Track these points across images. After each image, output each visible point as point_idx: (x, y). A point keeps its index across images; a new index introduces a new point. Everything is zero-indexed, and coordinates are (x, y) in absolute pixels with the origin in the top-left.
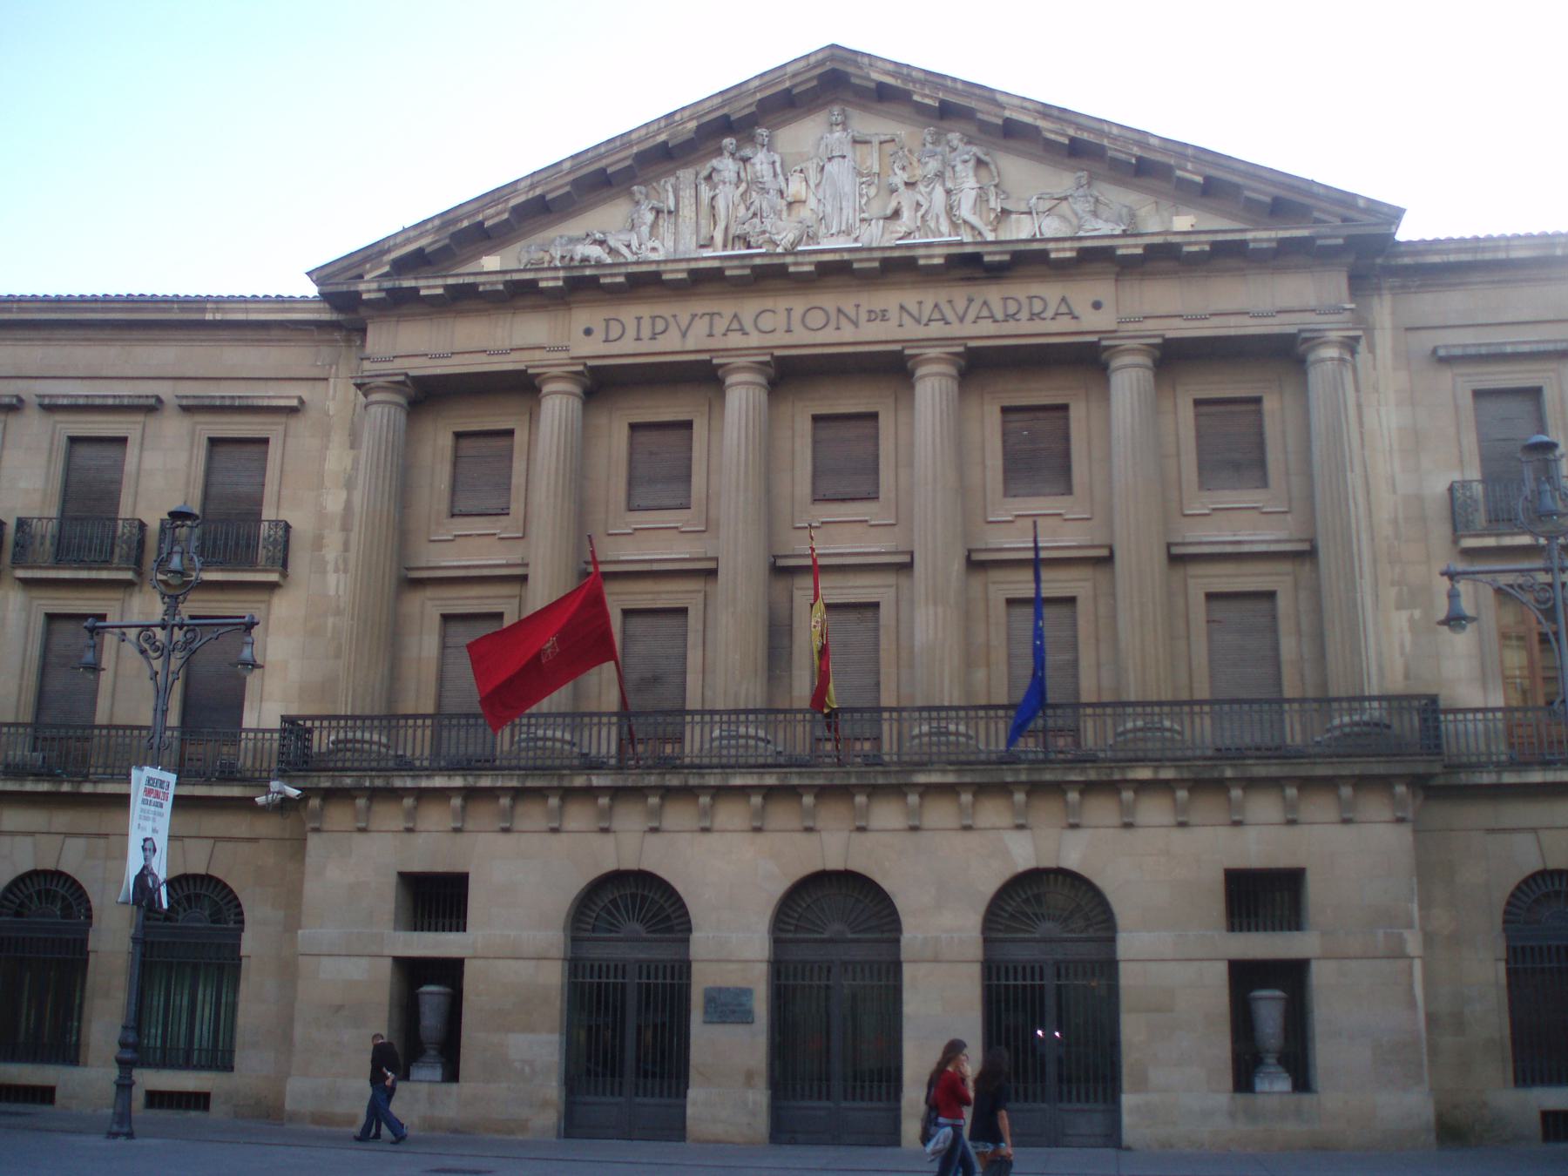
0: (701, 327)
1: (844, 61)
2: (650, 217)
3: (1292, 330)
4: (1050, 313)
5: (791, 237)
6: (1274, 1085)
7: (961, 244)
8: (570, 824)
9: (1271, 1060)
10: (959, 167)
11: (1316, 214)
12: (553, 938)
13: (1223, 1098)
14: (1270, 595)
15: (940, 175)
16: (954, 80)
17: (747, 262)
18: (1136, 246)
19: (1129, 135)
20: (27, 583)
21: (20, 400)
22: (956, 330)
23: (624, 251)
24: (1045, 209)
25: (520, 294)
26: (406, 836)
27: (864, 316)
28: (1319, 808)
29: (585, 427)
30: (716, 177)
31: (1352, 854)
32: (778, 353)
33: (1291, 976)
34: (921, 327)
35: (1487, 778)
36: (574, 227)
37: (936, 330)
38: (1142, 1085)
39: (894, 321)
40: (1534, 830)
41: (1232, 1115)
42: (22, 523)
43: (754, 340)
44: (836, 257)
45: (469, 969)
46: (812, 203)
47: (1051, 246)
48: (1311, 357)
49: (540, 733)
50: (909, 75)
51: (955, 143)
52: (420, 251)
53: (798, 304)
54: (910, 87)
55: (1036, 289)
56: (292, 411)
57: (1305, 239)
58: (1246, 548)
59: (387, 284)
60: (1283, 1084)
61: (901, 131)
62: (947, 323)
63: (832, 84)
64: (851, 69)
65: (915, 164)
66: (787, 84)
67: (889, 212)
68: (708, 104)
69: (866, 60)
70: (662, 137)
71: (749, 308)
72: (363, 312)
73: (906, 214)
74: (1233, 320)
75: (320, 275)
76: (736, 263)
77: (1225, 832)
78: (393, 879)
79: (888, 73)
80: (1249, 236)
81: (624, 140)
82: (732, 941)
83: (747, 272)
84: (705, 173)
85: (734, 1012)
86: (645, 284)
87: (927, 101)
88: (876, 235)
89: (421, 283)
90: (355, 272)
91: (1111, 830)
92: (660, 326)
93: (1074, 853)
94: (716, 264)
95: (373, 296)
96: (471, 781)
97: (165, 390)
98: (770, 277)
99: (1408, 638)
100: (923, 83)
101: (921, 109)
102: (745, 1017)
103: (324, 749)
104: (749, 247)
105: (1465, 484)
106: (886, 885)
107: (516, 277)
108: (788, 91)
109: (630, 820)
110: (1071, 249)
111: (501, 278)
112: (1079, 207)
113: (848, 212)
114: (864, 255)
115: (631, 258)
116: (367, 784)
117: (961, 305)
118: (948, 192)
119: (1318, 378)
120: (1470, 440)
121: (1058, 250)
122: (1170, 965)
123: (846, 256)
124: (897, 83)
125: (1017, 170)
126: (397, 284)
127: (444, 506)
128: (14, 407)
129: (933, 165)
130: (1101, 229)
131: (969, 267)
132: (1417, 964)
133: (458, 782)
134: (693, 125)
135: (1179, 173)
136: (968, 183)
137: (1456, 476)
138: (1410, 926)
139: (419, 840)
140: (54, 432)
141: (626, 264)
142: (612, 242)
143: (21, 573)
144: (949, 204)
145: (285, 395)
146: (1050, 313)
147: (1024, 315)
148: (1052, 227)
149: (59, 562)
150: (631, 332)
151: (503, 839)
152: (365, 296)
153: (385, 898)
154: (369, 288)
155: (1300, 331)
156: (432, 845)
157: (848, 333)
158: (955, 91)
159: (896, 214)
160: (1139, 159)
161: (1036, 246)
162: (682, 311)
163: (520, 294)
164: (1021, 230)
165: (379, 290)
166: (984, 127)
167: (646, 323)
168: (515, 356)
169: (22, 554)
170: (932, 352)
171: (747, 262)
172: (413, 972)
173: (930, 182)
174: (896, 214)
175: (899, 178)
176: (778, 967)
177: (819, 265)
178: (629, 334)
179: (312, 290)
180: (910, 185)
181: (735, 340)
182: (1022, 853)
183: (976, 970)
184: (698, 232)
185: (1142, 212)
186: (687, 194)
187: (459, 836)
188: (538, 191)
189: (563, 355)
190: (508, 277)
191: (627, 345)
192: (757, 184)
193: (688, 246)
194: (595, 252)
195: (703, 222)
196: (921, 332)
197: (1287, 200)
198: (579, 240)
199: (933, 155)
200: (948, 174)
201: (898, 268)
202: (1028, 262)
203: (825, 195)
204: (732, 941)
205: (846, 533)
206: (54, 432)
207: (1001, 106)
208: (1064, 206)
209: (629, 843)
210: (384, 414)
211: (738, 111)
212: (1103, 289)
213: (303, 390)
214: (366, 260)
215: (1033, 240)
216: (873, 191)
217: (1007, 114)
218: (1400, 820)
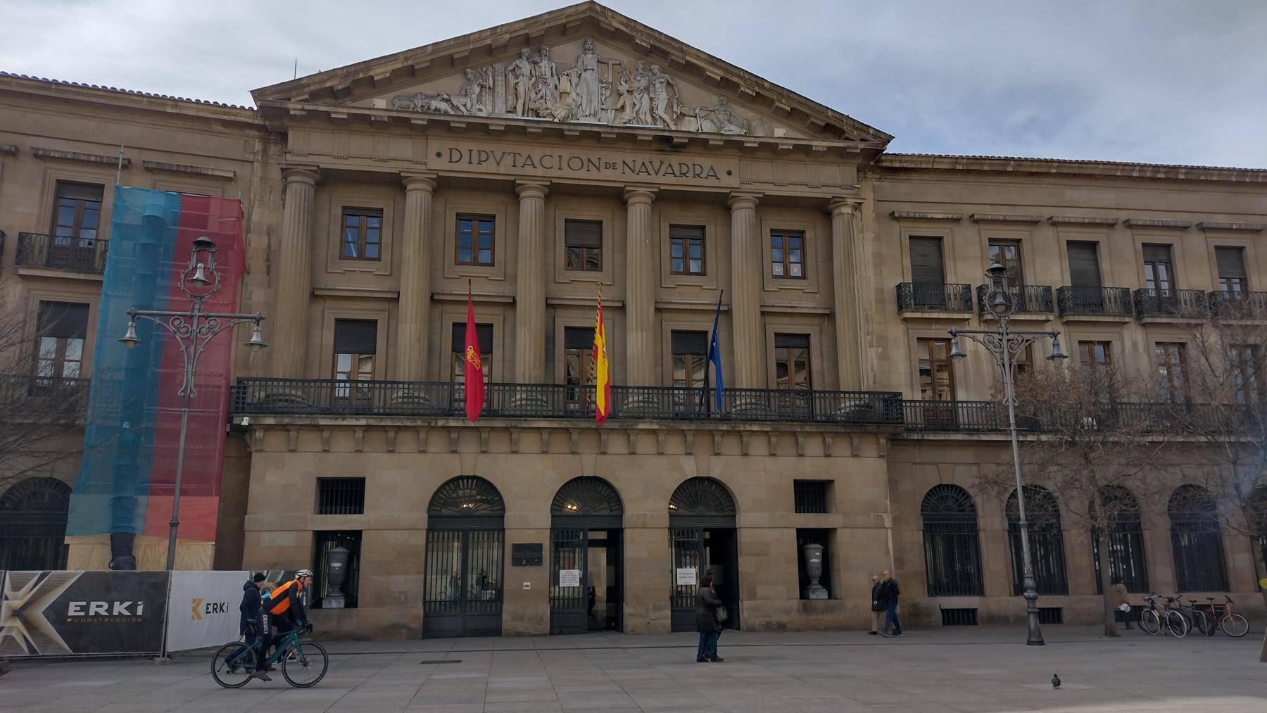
0: (508, 160)
2: (477, 90)
3: (829, 196)
4: (704, 175)
5: (563, 114)
6: (819, 594)
7: (657, 129)
8: (432, 449)
9: (815, 582)
10: (658, 85)
14: (807, 336)
15: (647, 89)
16: (661, 33)
20: (25, 278)
21: (17, 149)
22: (653, 178)
23: (462, 108)
24: (703, 117)
25: (399, 125)
27: (603, 166)
28: (842, 448)
29: (315, 202)
30: (518, 72)
31: (859, 474)
32: (554, 181)
33: (823, 537)
35: (915, 437)
36: (427, 88)
37: (643, 177)
38: (753, 595)
39: (620, 170)
40: (937, 464)
42: (22, 237)
43: (540, 172)
46: (574, 95)
48: (836, 212)
49: (416, 394)
51: (656, 71)
53: (566, 153)
55: (697, 160)
56: (230, 179)
58: (797, 311)
60: (823, 594)
61: (626, 59)
67: (619, 106)
68: (517, 26)
70: (488, 42)
71: (537, 152)
72: (286, 122)
73: (628, 109)
74: (799, 188)
75: (257, 94)
76: (609, 130)
78: (314, 483)
79: (622, 24)
80: (814, 143)
81: (465, 39)
84: (511, 68)
86: (479, 130)
88: (608, 118)
92: (484, 157)
93: (716, 469)
97: (133, 155)
98: (557, 135)
99: (875, 362)
101: (637, 47)
103: (256, 400)
104: (538, 116)
105: (906, 284)
106: (616, 484)
108: (564, 25)
109: (469, 446)
112: (721, 117)
113: (595, 104)
114: (609, 130)
115: (466, 113)
117: (657, 165)
118: (651, 99)
119: (838, 224)
120: (907, 262)
122: (766, 530)
124: (627, 31)
125: (688, 89)
127: (337, 253)
128: (14, 153)
129: (644, 83)
130: (733, 130)
131: (666, 143)
132: (890, 532)
133: (363, 422)
134: (507, 36)
136: (662, 97)
137: (900, 281)
140: (45, 174)
141: (463, 116)
142: (454, 102)
143: (23, 272)
144: (650, 106)
145: (225, 170)
146: (704, 175)
147: (690, 174)
148: (707, 126)
149: (48, 265)
150: (466, 158)
151: (387, 457)
152: (292, 112)
153: (310, 495)
154: (294, 107)
156: (340, 462)
157: (594, 174)
159: (623, 107)
162: (497, 148)
163: (399, 125)
164: (690, 125)
165: (303, 110)
166: (674, 64)
167: (475, 154)
168: (392, 164)
169: (23, 255)
170: (641, 190)
172: (805, 537)
173: (641, 92)
174: (623, 107)
175: (623, 88)
178: (467, 160)
179: (250, 103)
180: (630, 92)
181: (529, 171)
182: (690, 468)
184: (506, 102)
186: (500, 79)
188: (410, 63)
189: (423, 167)
192: (541, 78)
193: (500, 110)
194: (444, 106)
195: (510, 97)
196: (634, 178)
198: (432, 97)
199: (642, 75)
200: (651, 89)
201: (627, 139)
202: (698, 144)
203: (582, 92)
205: (584, 288)
206: (45, 174)
208: (712, 115)
210: (299, 190)
211: (534, 32)
212: (732, 164)
213: (236, 167)
214: (291, 90)
215: (697, 133)
216: (608, 93)
218: (881, 457)
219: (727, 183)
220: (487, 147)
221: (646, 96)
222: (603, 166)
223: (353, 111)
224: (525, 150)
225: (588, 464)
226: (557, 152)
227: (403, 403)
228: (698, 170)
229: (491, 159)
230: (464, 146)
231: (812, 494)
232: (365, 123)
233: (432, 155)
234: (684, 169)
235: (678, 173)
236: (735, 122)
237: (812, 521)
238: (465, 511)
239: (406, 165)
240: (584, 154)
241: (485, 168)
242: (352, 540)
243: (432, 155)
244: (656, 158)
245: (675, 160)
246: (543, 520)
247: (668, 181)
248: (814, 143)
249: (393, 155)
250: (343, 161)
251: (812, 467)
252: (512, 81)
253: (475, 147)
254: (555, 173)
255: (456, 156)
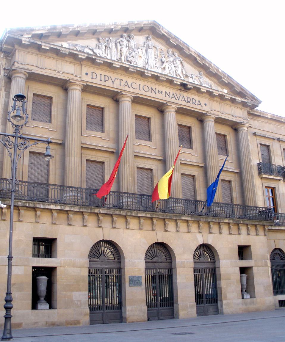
1: (156, 25)
2: (104, 47)
11: (247, 97)
12: (85, 261)
13: (241, 300)
15: (173, 62)
17: (135, 68)
18: (217, 93)
19: (215, 67)
24: (195, 77)
26: (36, 224)
34: (170, 98)
41: (242, 304)
43: (131, 90)
44: (156, 74)
45: (59, 272)
47: (146, 71)
50: (171, 35)
52: (42, 34)
53: (142, 83)
54: (170, 38)
55: (194, 97)
57: (76, 54)
58: (229, 170)
59: (32, 41)
62: (176, 99)
63: (153, 31)
64: (157, 28)
65: (167, 57)
66: (143, 26)
69: (161, 27)
71: (130, 81)
76: (133, 68)
77: (237, 236)
80: (237, 98)
82: (135, 263)
83: (135, 71)
84: (118, 41)
85: (137, 283)
87: (173, 43)
89: (43, 44)
90: (21, 33)
91: (217, 235)
93: (210, 240)
94: (128, 66)
95: (26, 43)
96: (63, 208)
100: (174, 38)
102: (140, 284)
107: (73, 52)
110: (150, 74)
111: (68, 50)
116: (27, 205)
121: (116, 64)
123: (159, 75)
124: (168, 36)
126: (35, 42)
133: (59, 208)
135: (223, 79)
138: (268, 260)
139: (40, 226)
144: (176, 69)
146: (196, 104)
151: (68, 228)
155: (242, 122)
157: (153, 95)
158: (180, 43)
160: (216, 73)
161: (199, 86)
165: (29, 42)
171: (135, 68)
172: (37, 271)
176: (147, 270)
177: (152, 75)
181: (126, 88)
183: (192, 270)
185: (213, 85)
187: (54, 225)
190: (70, 51)
191: (97, 81)
194: (90, 52)
196: (170, 100)
197: (242, 93)
203: (147, 56)
204: (135, 263)
207: (190, 50)
209: (108, 231)
217: (191, 53)
219: (205, 109)
220: (109, 74)
221: (173, 66)
222: (157, 92)
223: (52, 46)
224: (125, 79)
225: (161, 237)
226: (138, 82)
227: (75, 199)
228: (194, 102)
229: (110, 80)
230: (98, 72)
231: (243, 251)
232: (57, 53)
233: (84, 74)
234: (189, 100)
235: (187, 101)
236: (207, 83)
237: (44, 262)
238: (106, 258)
239: (71, 77)
240: (150, 85)
241: (107, 84)
242: (49, 272)
243: (84, 74)
244: (178, 93)
245: (185, 95)
246: (141, 264)
247: (184, 104)
248: (237, 98)
249: (65, 71)
250: (42, 70)
251: (243, 240)
252: (119, 47)
253: (103, 73)
254: (137, 91)
255: (94, 76)
